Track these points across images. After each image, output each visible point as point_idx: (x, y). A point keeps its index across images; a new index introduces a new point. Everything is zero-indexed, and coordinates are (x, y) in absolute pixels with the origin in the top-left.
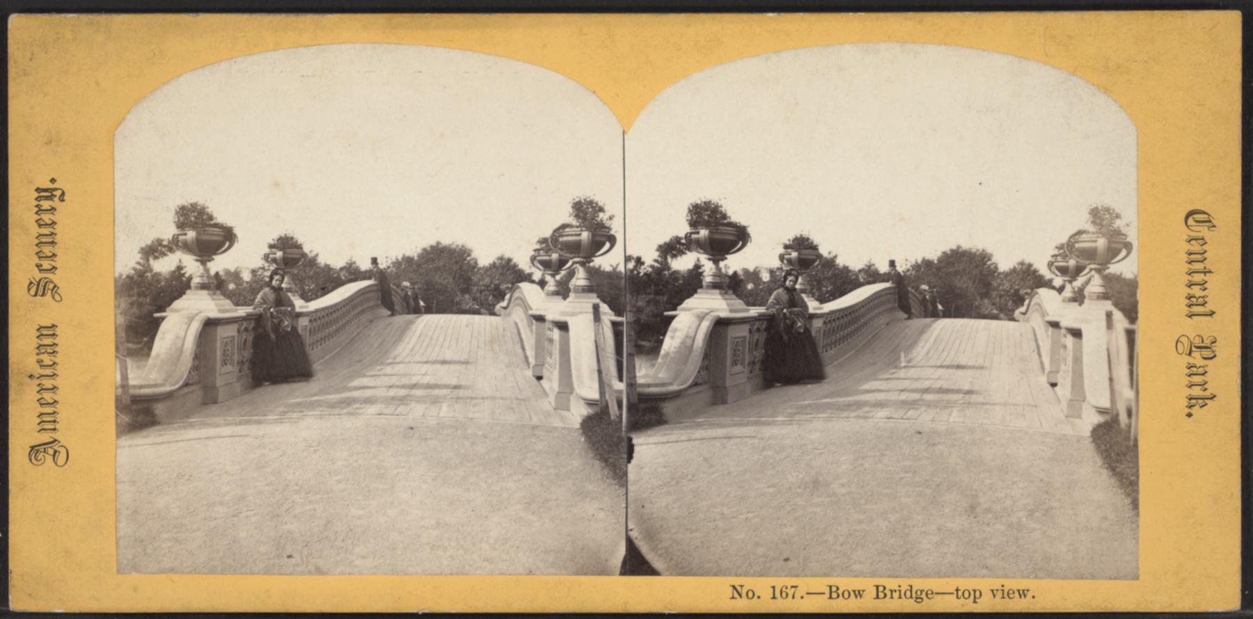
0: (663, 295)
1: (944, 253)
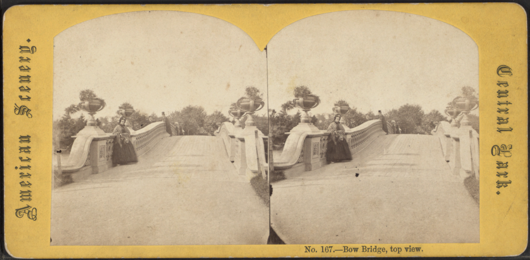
0: (284, 125)
1: (401, 107)
